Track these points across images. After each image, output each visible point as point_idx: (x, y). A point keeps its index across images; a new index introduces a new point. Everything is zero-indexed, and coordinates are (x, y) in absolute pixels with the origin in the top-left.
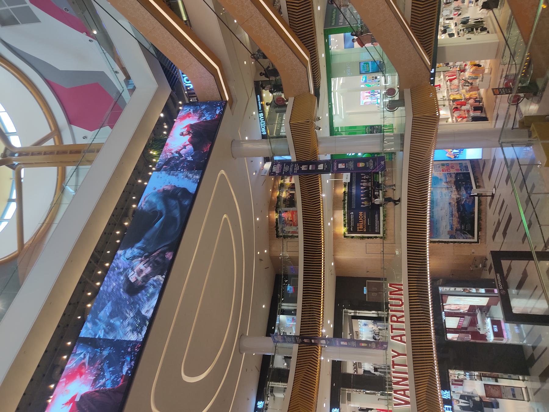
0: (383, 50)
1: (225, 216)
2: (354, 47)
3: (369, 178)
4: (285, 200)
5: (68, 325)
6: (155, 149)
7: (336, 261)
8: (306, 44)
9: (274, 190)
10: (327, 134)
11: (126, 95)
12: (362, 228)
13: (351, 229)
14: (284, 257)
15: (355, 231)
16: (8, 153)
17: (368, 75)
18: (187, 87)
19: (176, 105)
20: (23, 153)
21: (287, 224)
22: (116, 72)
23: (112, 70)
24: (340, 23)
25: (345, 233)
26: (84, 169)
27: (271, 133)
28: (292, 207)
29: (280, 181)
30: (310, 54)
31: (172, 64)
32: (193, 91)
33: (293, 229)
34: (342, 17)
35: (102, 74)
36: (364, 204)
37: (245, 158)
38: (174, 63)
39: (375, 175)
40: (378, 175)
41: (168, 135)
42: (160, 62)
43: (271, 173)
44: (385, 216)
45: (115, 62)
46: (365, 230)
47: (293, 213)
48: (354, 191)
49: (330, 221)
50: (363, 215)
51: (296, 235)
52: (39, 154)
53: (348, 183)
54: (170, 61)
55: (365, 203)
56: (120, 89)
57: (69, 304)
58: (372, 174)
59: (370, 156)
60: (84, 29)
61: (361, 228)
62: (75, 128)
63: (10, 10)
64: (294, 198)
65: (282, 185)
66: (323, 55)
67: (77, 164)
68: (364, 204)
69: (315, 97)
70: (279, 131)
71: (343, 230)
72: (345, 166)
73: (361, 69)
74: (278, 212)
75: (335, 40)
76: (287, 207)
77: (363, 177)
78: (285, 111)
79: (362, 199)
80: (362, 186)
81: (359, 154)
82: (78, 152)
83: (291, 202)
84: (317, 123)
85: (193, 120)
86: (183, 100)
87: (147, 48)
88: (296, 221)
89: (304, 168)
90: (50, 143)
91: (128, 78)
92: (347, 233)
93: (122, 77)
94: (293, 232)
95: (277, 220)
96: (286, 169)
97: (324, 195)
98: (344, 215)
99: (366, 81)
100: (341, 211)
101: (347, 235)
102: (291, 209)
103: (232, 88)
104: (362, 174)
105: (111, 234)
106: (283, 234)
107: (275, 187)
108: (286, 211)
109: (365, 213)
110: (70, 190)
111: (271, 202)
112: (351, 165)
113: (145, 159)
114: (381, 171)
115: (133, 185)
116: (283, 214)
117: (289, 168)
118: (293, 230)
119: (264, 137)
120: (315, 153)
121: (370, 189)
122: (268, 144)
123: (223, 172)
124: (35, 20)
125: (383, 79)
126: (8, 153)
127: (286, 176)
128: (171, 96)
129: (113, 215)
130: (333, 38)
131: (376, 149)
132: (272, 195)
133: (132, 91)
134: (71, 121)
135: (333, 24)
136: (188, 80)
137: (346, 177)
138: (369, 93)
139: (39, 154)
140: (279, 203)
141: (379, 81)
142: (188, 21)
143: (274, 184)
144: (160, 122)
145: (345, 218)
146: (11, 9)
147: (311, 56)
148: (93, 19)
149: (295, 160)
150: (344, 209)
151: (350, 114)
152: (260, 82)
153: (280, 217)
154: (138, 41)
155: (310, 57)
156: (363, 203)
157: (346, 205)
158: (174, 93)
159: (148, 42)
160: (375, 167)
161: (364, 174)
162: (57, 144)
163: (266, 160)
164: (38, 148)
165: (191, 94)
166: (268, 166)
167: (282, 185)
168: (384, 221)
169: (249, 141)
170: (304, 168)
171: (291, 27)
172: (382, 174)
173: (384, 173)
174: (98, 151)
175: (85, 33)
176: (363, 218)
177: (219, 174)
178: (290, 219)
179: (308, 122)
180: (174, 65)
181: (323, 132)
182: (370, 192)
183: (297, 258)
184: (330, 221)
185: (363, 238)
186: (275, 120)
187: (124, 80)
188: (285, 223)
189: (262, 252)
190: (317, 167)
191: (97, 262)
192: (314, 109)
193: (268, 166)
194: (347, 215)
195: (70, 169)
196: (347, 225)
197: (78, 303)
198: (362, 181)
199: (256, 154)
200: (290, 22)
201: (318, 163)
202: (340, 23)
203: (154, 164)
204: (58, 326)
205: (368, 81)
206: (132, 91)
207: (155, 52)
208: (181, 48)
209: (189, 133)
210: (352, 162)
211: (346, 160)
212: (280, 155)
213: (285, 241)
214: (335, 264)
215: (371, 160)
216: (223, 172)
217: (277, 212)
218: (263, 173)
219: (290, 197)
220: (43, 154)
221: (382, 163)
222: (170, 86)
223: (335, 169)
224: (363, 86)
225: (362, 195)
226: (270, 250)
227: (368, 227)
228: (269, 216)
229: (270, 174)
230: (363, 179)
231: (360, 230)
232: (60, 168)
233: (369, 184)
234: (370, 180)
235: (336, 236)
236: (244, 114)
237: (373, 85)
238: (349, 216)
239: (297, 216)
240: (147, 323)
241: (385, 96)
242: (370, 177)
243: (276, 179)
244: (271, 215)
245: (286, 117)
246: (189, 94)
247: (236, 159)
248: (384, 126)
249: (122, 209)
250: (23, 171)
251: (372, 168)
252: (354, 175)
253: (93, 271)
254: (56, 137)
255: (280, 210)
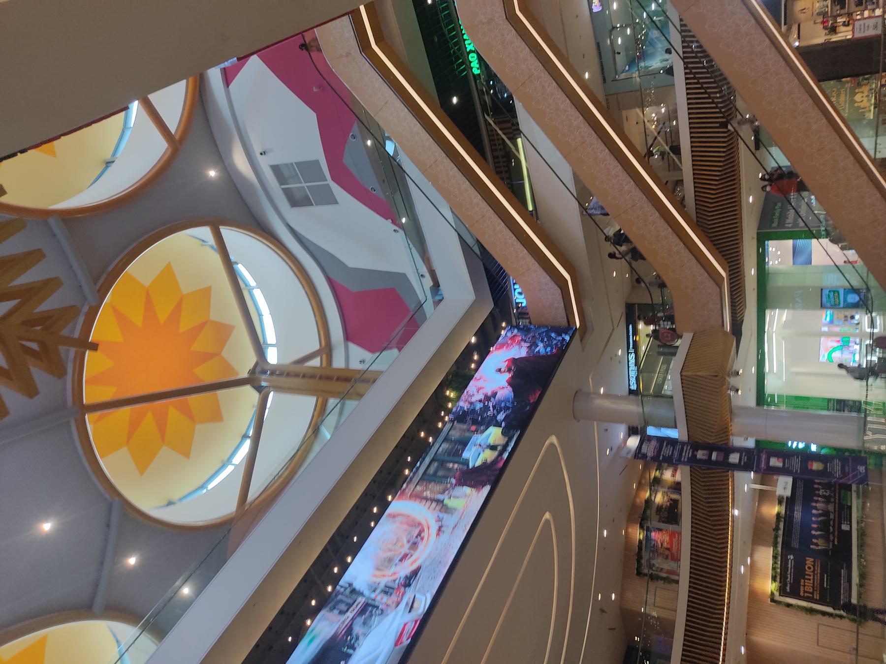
0: (869, 270)
1: (547, 516)
2: (811, 263)
3: (830, 496)
4: (660, 508)
5: (271, 648)
6: (454, 389)
7: (749, 645)
8: (723, 251)
9: (640, 486)
10: (752, 401)
11: (428, 307)
12: (811, 591)
13: (788, 588)
14: (646, 615)
15: (795, 594)
16: (258, 369)
17: (836, 312)
18: (517, 304)
19: (497, 329)
20: (277, 372)
21: (660, 554)
22: (422, 276)
23: (416, 271)
24: (789, 224)
25: (772, 593)
26: (351, 404)
27: (647, 387)
28: (672, 524)
29: (654, 473)
30: (730, 267)
31: (502, 268)
32: (524, 311)
33: (668, 565)
34: (791, 213)
35: (403, 277)
36: (817, 545)
37: (595, 423)
38: (505, 267)
39: (843, 491)
40: (849, 492)
41: (477, 370)
42: (484, 265)
43: (639, 454)
44: (863, 576)
45: (424, 262)
46: (817, 596)
47: (672, 535)
48: (798, 515)
49: (744, 563)
50: (814, 566)
51: (676, 578)
52: (297, 375)
53: (787, 498)
54: (499, 265)
55: (820, 541)
56: (421, 297)
57: (282, 612)
58: (837, 488)
59: (834, 453)
60: (387, 212)
61: (808, 590)
62: (352, 347)
63: (306, 187)
64: (677, 508)
65: (657, 482)
66: (753, 272)
67: (344, 396)
68: (817, 545)
69: (732, 336)
70: (660, 386)
71: (769, 586)
72: (784, 464)
73: (824, 300)
74: (645, 528)
75: (777, 250)
76: (663, 522)
77: (817, 492)
78: (674, 354)
79: (813, 532)
80: (816, 508)
81: (814, 448)
82: (347, 380)
83: (671, 514)
84: (733, 381)
85: (519, 351)
86: (509, 323)
87: (469, 244)
88: (677, 552)
89: (701, 454)
90: (316, 362)
91: (436, 286)
92: (777, 594)
93: (428, 282)
94: (669, 572)
95: (640, 541)
96: (667, 451)
97: (736, 512)
98: (775, 557)
99: (831, 322)
100: (767, 548)
101: (777, 597)
102: (671, 527)
103: (589, 309)
104: (816, 486)
105: (365, 510)
106: (651, 572)
107: (643, 481)
108: (660, 530)
109: (818, 564)
110: (326, 434)
111: (633, 507)
112: (796, 464)
113: (437, 401)
114: (858, 484)
115: (412, 440)
116: (653, 534)
117: (673, 451)
118: (669, 568)
119: (631, 392)
120: (725, 431)
121: (832, 517)
122: (638, 405)
123: (553, 439)
124: (333, 201)
125: (866, 319)
126: (258, 369)
127: (666, 465)
128: (491, 314)
129: (374, 481)
130: (772, 246)
131: (850, 443)
132: (637, 495)
133: (437, 303)
134: (349, 337)
135: (774, 225)
136: (520, 293)
137: (784, 486)
138: (838, 341)
139: (297, 375)
140: (648, 512)
141: (858, 324)
142: (534, 211)
143: (642, 476)
144: (469, 350)
145: (775, 563)
146: (302, 183)
147: (730, 271)
148: (406, 205)
149: (685, 438)
150: (775, 545)
151: (797, 374)
152: (636, 305)
153: (647, 538)
154: (458, 234)
155: (728, 271)
156: (815, 541)
157: (780, 540)
158: (497, 310)
159: (472, 237)
160: (844, 474)
161: (820, 487)
162: (324, 364)
163: (632, 431)
164: (298, 368)
165: (523, 313)
166: (633, 442)
167: (657, 482)
168: (861, 585)
169: (606, 396)
170: (701, 454)
171: (698, 225)
172: (858, 492)
173: (863, 488)
174: (374, 381)
175: (390, 220)
176: (813, 572)
177: (547, 442)
178: (665, 545)
179: (716, 376)
180: (504, 271)
181: (745, 396)
182: (832, 523)
183: (672, 624)
184: (744, 563)
185: (811, 611)
186: (656, 366)
187: (430, 287)
188: (654, 550)
189: (607, 597)
190: (727, 457)
191: (336, 552)
192: (729, 355)
193: (633, 442)
194: (779, 558)
195: (332, 402)
196: (778, 579)
197: (294, 614)
198: (816, 498)
199: (615, 418)
200: (697, 217)
201: (729, 450)
202: (789, 224)
203: (448, 412)
204: (257, 646)
205: (836, 322)
206: (437, 303)
207: (480, 250)
208: (518, 246)
209: (509, 370)
210: (798, 457)
211: (786, 454)
212: (658, 426)
213: (652, 586)
214: (747, 649)
215: (837, 461)
216: (553, 439)
217: (642, 527)
218: (623, 453)
219: (670, 504)
220: (301, 376)
221: (862, 469)
222: (493, 300)
223: (763, 465)
224: (825, 329)
225: (814, 526)
226: (621, 596)
227: (823, 591)
228: (626, 532)
229: (635, 456)
230: (819, 496)
231: (806, 594)
232: (320, 400)
233: (831, 507)
234: (832, 500)
235: (754, 596)
236: (603, 353)
237: (846, 329)
238: (784, 561)
239: (679, 542)
240: (783, 520)
241: (869, 349)
242: (832, 494)
243: (646, 467)
244: (630, 530)
245: (677, 363)
246: (520, 314)
247: (579, 421)
248: (866, 403)
249: (389, 474)
250: (271, 394)
251: (838, 474)
252: (800, 484)
253: (328, 566)
254: (324, 356)
255: (649, 524)
